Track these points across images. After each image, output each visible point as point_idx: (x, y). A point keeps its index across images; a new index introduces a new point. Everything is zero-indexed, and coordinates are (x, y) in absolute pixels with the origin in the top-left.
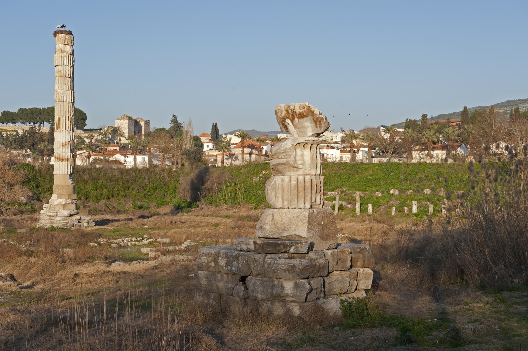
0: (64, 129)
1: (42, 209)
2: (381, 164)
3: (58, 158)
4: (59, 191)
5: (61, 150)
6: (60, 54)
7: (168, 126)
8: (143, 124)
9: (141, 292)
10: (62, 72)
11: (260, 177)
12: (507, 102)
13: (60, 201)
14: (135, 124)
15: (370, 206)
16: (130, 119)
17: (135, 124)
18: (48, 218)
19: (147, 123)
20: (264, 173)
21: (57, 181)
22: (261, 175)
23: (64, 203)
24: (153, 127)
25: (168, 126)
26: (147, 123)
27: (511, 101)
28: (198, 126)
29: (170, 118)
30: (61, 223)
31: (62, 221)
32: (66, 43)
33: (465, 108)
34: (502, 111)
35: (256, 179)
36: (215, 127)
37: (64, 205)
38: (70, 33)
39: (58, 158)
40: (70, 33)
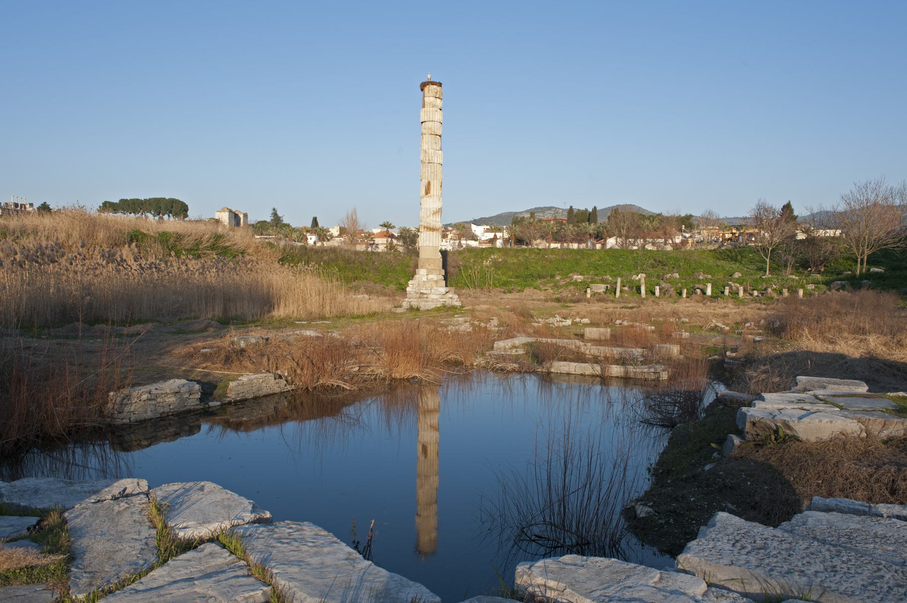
2: (579, 250)
7: (268, 218)
8: (241, 216)
9: (39, 337)
13: (430, 276)
14: (235, 217)
16: (230, 211)
17: (235, 217)
19: (245, 216)
23: (435, 279)
24: (252, 219)
25: (268, 218)
26: (245, 216)
28: (296, 219)
29: (271, 211)
33: (571, 207)
37: (437, 282)
38: (440, 85)
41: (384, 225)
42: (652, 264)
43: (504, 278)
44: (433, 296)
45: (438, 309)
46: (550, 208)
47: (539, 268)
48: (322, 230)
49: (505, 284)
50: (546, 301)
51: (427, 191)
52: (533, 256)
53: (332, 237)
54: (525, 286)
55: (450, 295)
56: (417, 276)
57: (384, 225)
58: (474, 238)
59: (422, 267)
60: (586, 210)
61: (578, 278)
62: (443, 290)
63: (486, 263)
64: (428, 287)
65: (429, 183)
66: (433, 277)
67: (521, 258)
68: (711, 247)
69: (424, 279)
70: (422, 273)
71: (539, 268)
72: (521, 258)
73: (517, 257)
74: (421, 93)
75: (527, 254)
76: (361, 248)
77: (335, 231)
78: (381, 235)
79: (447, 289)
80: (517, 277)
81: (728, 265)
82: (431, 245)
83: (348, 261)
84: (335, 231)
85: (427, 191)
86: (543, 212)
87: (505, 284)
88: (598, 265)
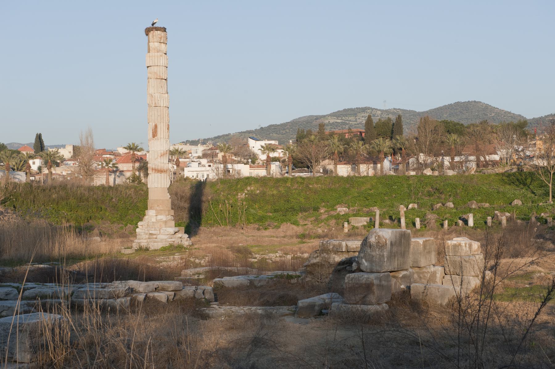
0: (162, 137)
1: (137, 227)
3: (155, 170)
4: (158, 206)
5: (159, 160)
6: (156, 53)
10: (158, 73)
11: (246, 194)
12: (345, 110)
13: (159, 217)
15: (446, 223)
18: (147, 236)
20: (249, 188)
21: (152, 196)
22: (246, 192)
23: (164, 219)
27: (349, 110)
30: (168, 242)
31: (170, 240)
32: (162, 41)
34: (340, 121)
35: (242, 196)
36: (39, 137)
37: (166, 222)
38: (164, 30)
39: (155, 170)
40: (164, 30)
41: (129, 148)
42: (429, 192)
43: (261, 213)
44: (161, 237)
45: (164, 249)
46: (364, 110)
47: (302, 200)
48: (49, 155)
49: (261, 219)
50: (284, 237)
51: (155, 134)
52: (296, 186)
53: (63, 160)
54: (283, 221)
55: (179, 235)
56: (146, 217)
57: (129, 148)
58: (252, 159)
59: (151, 209)
60: (389, 119)
61: (342, 210)
62: (172, 230)
63: (242, 196)
64: (157, 229)
65: (156, 126)
66: (163, 217)
67: (281, 189)
68: (500, 170)
69: (154, 220)
70: (151, 214)
71: (302, 200)
72: (281, 189)
73: (277, 188)
74: (146, 37)
75: (289, 184)
76: (100, 180)
77: (66, 153)
78: (125, 159)
79: (177, 229)
80: (276, 211)
81: (508, 189)
82: (158, 185)
83: (81, 199)
84: (66, 153)
85: (155, 134)
86: (355, 115)
87: (261, 219)
88: (369, 195)
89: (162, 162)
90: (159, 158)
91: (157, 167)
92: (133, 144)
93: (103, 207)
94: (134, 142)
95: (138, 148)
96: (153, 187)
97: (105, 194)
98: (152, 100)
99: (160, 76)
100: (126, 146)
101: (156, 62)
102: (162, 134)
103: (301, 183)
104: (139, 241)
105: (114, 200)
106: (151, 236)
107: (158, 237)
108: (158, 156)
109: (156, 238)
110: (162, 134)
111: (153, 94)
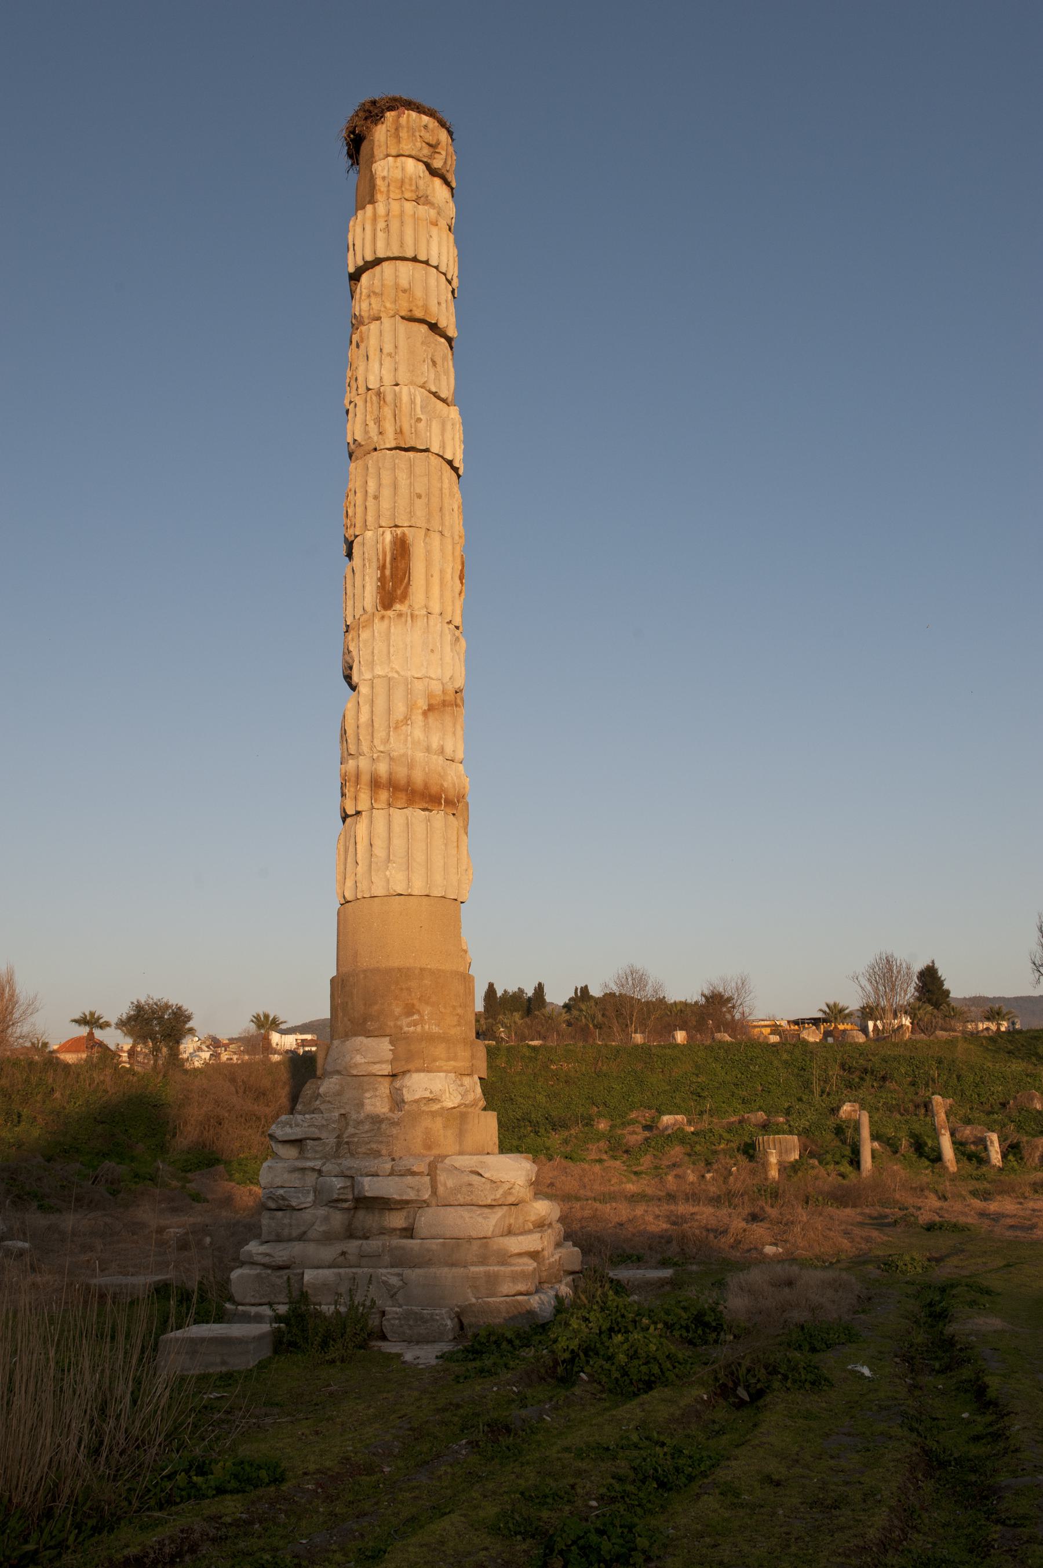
5: (418, 733)
6: (409, 206)
10: (419, 293)
18: (338, 1219)
23: (451, 1101)
32: (437, 164)
41: (83, 1021)
47: (541, 1099)
51: (394, 588)
57: (83, 1021)
65: (402, 549)
89: (435, 745)
90: (418, 718)
91: (401, 773)
92: (92, 1014)
93: (25, 1112)
94: (93, 1010)
95: (101, 1021)
96: (379, 890)
97: (34, 1079)
98: (378, 421)
99: (426, 308)
100: (77, 1017)
101: (409, 240)
102: (436, 590)
103: (530, 1058)
104: (281, 1253)
105: (57, 1095)
106: (366, 1219)
107: (425, 1220)
108: (411, 707)
109: (409, 1232)
110: (436, 590)
111: (388, 391)
